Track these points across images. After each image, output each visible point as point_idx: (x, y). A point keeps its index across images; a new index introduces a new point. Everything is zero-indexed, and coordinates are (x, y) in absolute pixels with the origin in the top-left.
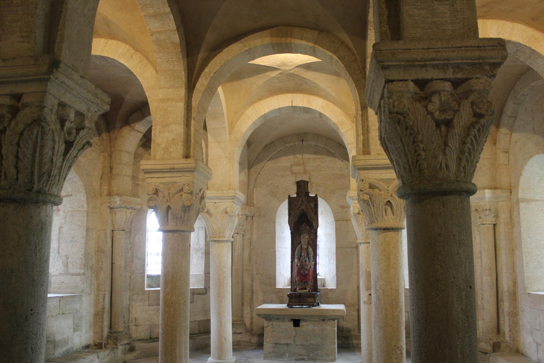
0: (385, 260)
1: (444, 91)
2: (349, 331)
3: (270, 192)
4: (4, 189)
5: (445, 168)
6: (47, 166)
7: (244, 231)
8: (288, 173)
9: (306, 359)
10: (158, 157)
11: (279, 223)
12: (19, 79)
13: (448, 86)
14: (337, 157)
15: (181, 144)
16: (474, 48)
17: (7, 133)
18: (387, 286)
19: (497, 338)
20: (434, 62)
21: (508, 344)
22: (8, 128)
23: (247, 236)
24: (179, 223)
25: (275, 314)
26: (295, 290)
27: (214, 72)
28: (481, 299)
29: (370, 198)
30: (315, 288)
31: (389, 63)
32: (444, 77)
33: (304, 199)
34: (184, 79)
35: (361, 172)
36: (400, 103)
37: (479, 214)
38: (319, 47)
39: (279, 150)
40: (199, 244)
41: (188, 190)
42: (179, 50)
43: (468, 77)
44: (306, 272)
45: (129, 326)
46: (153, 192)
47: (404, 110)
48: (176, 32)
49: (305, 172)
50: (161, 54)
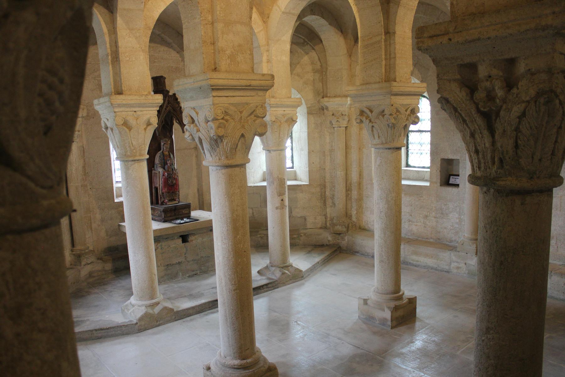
3: (97, 86)
9: (199, 273)
18: (397, 197)
21: (354, 223)
25: (168, 233)
28: (329, 191)
35: (392, 97)
41: (262, 113)
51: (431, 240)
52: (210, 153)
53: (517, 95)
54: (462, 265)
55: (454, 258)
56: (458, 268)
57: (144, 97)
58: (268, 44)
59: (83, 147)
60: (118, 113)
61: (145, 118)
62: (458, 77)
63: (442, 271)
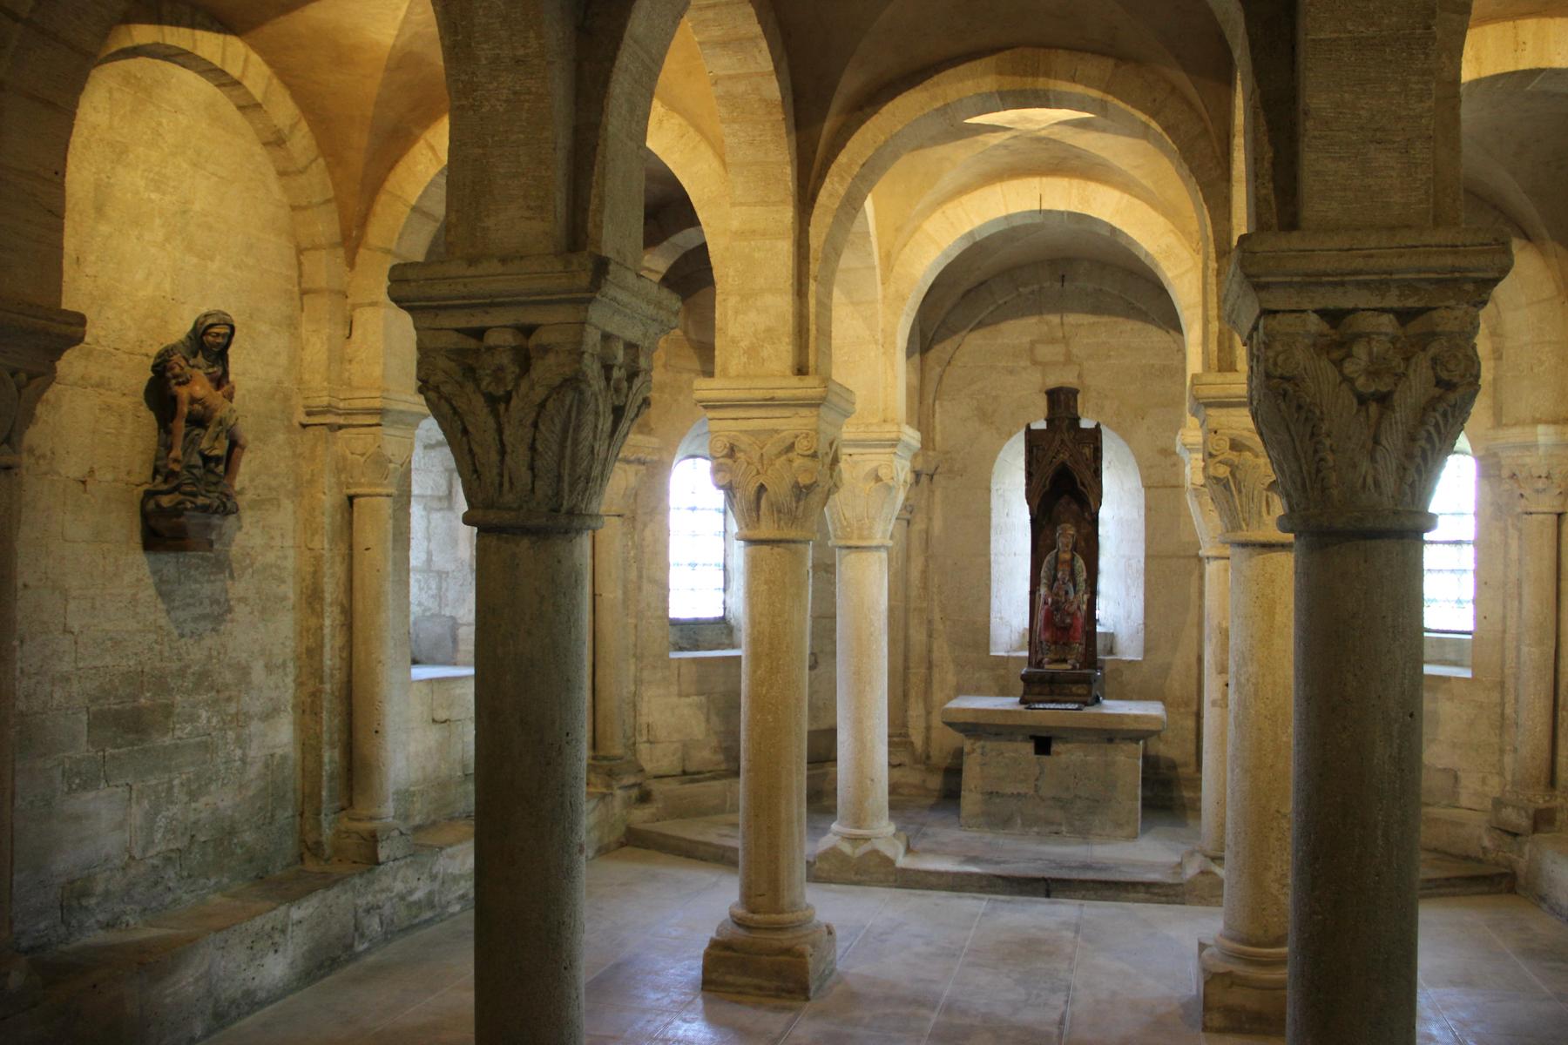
0: (1263, 618)
1: (1379, 334)
2: (1173, 766)
4: (510, 509)
5: (1372, 487)
6: (586, 463)
7: (911, 513)
8: (1022, 364)
10: (732, 371)
11: (1000, 492)
13: (1387, 323)
14: (1152, 322)
15: (787, 340)
16: (1443, 249)
17: (514, 403)
18: (1264, 675)
19: (1547, 798)
20: (1361, 278)
22: (514, 393)
23: (918, 526)
24: (786, 524)
26: (1039, 664)
27: (861, 163)
29: (1233, 474)
30: (1090, 659)
31: (1270, 279)
32: (1379, 306)
33: (1066, 437)
34: (790, 184)
35: (1211, 412)
36: (1287, 359)
37: (1520, 487)
38: (1116, 102)
39: (1000, 302)
42: (781, 117)
43: (1430, 305)
44: (1068, 621)
45: (634, 744)
46: (724, 452)
47: (1296, 372)
48: (774, 77)
49: (1069, 360)
50: (736, 126)
61: (869, 467)
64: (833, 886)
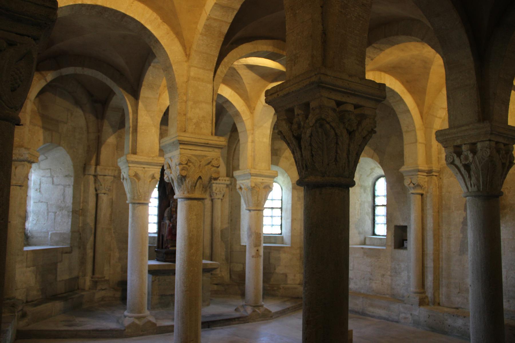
12: (367, 96)
40: (64, 202)
41: (216, 164)
50: (205, 37)
51: (388, 296)
52: (178, 189)
53: (308, 123)
54: (409, 315)
55: (402, 309)
56: (405, 318)
57: (151, 158)
58: (253, 130)
59: (112, 200)
60: (131, 168)
61: (151, 173)
62: (286, 117)
63: (392, 321)
64: (134, 338)
